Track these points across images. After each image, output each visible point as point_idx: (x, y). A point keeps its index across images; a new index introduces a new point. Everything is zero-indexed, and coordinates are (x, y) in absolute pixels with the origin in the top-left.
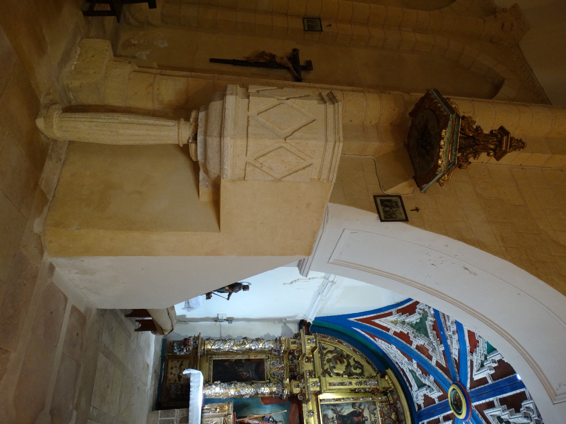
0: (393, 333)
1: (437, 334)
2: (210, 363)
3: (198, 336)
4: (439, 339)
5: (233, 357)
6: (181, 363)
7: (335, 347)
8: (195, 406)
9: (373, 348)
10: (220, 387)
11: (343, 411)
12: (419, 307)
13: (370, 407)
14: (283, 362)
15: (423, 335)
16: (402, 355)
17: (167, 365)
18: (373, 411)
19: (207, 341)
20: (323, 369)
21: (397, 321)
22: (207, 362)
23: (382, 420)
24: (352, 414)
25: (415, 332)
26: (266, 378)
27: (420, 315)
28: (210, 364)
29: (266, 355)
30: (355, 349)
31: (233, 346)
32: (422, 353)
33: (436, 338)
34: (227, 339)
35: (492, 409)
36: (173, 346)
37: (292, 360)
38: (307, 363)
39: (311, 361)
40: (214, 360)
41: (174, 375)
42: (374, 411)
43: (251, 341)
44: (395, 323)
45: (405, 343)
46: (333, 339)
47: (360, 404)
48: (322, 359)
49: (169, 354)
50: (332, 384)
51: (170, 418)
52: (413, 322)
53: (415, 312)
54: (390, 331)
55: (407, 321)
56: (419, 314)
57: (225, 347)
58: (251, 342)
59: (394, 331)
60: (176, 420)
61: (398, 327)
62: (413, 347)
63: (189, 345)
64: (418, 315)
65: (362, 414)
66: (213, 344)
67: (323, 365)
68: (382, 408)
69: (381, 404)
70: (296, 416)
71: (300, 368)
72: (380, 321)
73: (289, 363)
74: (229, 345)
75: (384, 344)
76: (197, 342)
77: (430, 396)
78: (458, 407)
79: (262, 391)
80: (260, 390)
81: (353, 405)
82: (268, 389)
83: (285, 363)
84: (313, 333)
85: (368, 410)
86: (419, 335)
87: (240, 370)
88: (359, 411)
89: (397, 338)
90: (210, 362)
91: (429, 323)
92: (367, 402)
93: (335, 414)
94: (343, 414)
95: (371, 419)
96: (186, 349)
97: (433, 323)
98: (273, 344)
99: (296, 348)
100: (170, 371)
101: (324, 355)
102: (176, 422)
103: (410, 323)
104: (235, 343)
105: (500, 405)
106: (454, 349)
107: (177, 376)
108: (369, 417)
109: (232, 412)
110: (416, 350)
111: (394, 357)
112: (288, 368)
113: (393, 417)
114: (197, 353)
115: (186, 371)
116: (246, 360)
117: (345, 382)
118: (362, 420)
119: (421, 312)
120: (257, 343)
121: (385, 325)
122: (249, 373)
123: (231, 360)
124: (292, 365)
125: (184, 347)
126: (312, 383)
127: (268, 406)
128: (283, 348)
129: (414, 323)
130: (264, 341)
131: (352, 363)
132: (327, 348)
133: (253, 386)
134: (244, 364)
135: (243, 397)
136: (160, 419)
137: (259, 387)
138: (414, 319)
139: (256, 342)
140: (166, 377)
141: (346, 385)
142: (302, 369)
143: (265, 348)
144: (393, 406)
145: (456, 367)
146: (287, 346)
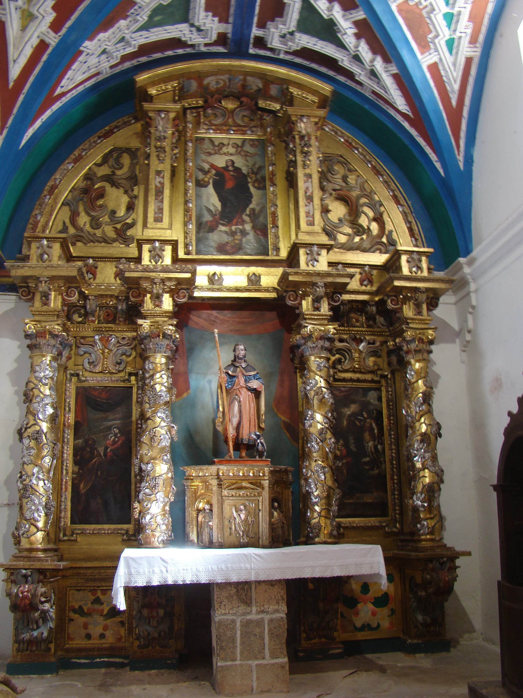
0: (52, 34)
2: (79, 532)
3: (6, 569)
5: (66, 469)
6: (75, 611)
7: (63, 204)
8: (215, 567)
9: (77, 112)
10: (149, 500)
11: (212, 208)
14: (90, 339)
16: (111, 31)
17: (80, 652)
18: (215, 146)
19: (22, 544)
20: (114, 240)
21: (23, 11)
22: (76, 541)
24: (218, 187)
26: (127, 385)
28: (82, 533)
29: (68, 382)
30: (74, 157)
31: (41, 467)
34: (21, 486)
36: (31, 642)
37: (86, 315)
38: (98, 276)
39: (93, 266)
40: (73, 522)
41: (105, 628)
42: (216, 143)
43: (31, 417)
46: (41, 206)
47: (199, 169)
48: (92, 239)
49: (53, 650)
50: (156, 215)
51: (239, 633)
54: (47, 40)
57: (42, 491)
58: (35, 415)
59: (50, 27)
60: (244, 614)
61: (41, 11)
63: (32, 595)
65: (221, 170)
66: (32, 524)
67: (106, 240)
68: (211, 126)
69: (202, 126)
70: (216, 317)
71: (110, 293)
72: (14, 61)
73: (93, 322)
74: (39, 479)
75: (75, 75)
76: (24, 571)
79: (164, 389)
80: (161, 396)
81: (200, 184)
82: (158, 375)
83: (91, 334)
84: (20, 252)
85: (212, 156)
87: (101, 450)
88: (215, 175)
89: (69, 24)
90: (77, 534)
92: (195, 153)
93: (218, 226)
94: (218, 210)
95: (231, 155)
96: (42, 603)
98: (44, 356)
99: (60, 297)
100: (95, 642)
101: (81, 234)
102: (249, 613)
104: (32, 463)
107: (109, 621)
108: (227, 158)
109: (213, 469)
111: (109, 61)
112: (105, 325)
113: (230, 105)
114: (55, 571)
115: (119, 601)
116: (77, 435)
117: (156, 186)
118: (232, 173)
120: (38, 399)
121: (28, 51)
122: (109, 428)
123: (74, 476)
124: (99, 316)
125: (38, 610)
126: (152, 261)
127: (194, 381)
128: (57, 328)
130: (33, 380)
131: (104, 171)
132: (64, 223)
133: (149, 415)
134: (86, 441)
135: (176, 439)
136: (238, 658)
137: (157, 396)
139: (34, 401)
140: (112, 651)
141: (163, 183)
142: (111, 290)
143: (52, 378)
144: (210, 101)
146: (51, 318)
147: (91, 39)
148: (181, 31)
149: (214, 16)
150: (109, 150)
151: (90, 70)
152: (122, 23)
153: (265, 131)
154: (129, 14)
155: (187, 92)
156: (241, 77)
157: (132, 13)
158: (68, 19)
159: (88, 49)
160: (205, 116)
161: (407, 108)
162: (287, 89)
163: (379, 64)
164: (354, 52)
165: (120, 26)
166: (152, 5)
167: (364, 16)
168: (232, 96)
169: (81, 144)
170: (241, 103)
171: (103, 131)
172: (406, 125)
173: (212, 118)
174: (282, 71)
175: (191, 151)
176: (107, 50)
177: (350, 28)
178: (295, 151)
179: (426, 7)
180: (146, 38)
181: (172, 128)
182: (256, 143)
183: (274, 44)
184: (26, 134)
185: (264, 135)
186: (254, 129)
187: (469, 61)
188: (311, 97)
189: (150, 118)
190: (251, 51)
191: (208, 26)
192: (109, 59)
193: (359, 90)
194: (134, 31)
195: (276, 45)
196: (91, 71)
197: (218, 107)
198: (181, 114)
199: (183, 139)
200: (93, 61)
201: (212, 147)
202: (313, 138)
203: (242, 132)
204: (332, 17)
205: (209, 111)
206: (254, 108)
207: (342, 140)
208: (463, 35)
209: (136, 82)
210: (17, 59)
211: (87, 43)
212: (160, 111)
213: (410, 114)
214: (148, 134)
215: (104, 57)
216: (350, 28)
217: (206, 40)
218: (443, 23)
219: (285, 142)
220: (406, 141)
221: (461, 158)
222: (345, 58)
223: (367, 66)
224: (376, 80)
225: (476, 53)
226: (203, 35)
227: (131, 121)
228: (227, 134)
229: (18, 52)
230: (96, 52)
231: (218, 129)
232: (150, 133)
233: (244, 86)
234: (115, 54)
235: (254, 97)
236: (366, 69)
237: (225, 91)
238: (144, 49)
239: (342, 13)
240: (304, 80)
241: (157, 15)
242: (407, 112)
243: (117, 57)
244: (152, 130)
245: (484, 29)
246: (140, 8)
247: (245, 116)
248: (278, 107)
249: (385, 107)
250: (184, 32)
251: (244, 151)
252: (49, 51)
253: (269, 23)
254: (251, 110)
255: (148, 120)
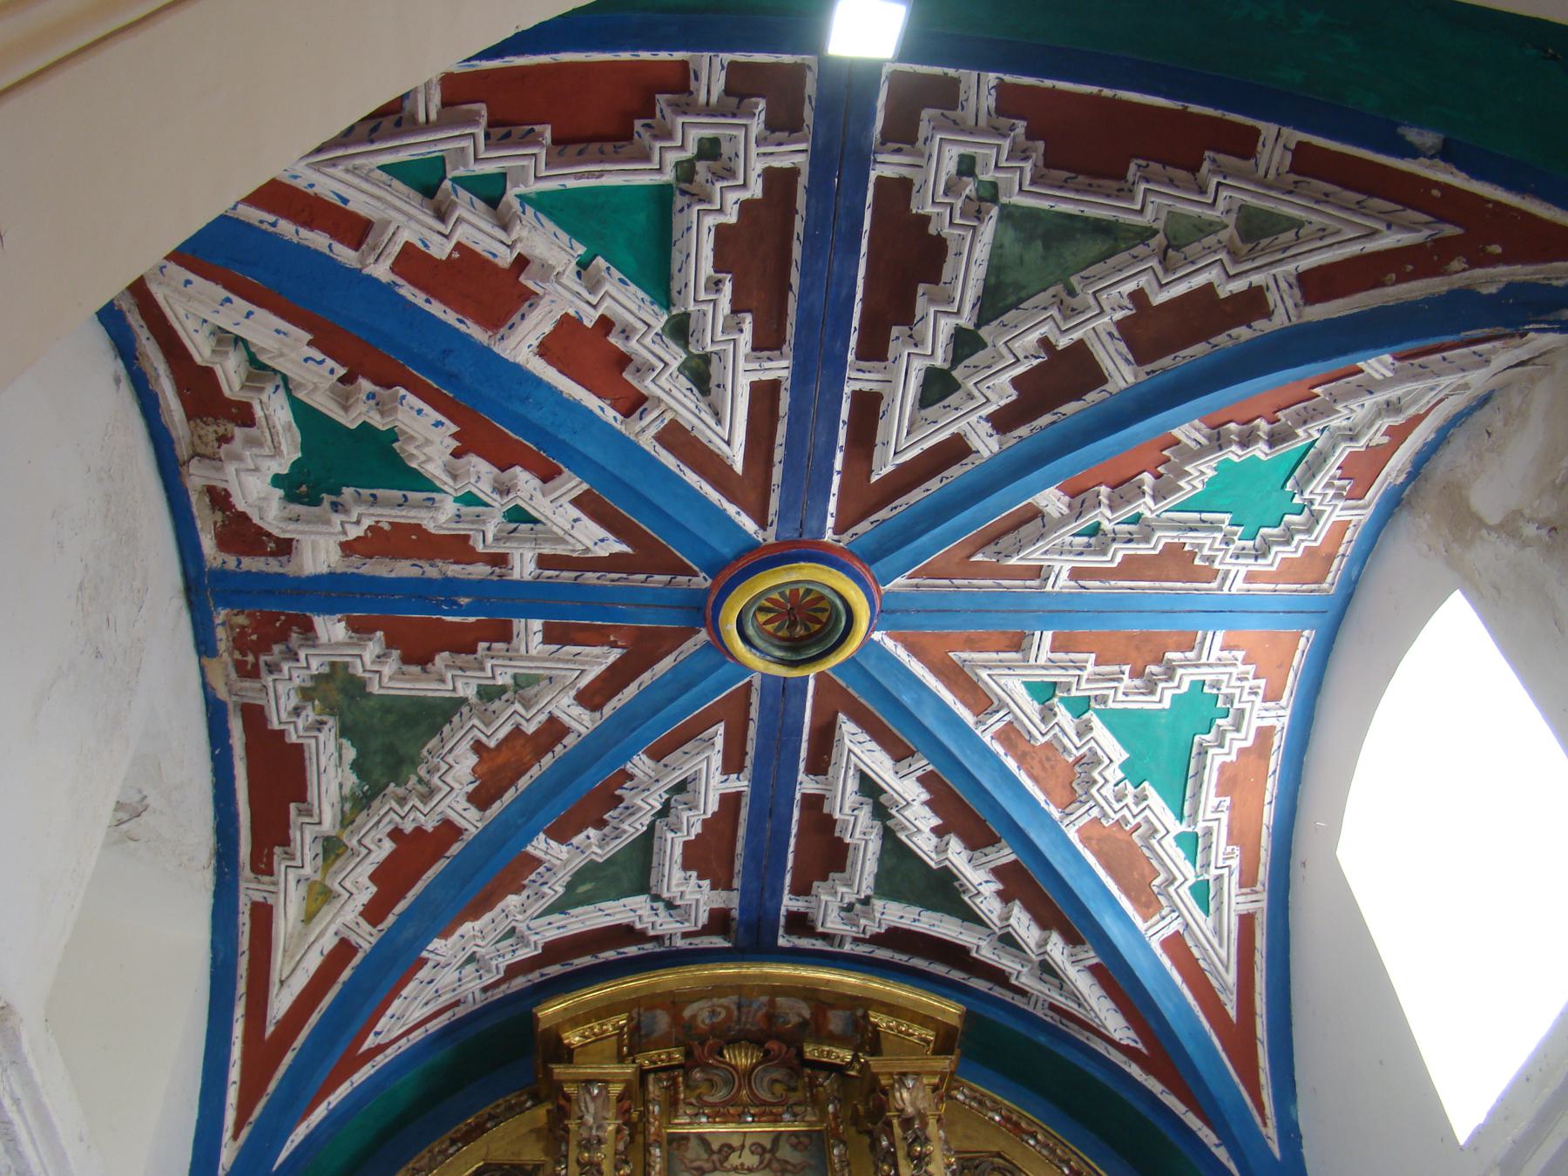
1: (456, 650)
4: (482, 645)
12: (284, 716)
13: (696, 1164)
15: (429, 746)
16: (487, 917)
18: (712, 1152)
23: (753, 1116)
25: (401, 791)
27: (326, 728)
32: (513, 781)
33: (471, 657)
35: (881, 423)
42: (715, 1147)
44: (320, 896)
45: (441, 865)
52: (347, 791)
53: (299, 748)
54: (354, 939)
55: (329, 822)
56: (319, 730)
59: (362, 914)
62: (471, 821)
64: (322, 737)
72: (282, 982)
77: (709, 816)
78: (810, 636)
86: (422, 771)
89: (401, 907)
91: (387, 670)
97: (396, 653)
103: (342, 811)
105: (883, 364)
106: (573, 527)
110: (488, 812)
111: (480, 977)
113: (742, 1059)
119: (310, 714)
121: (313, 962)
129: (352, 779)
138: (332, 770)
144: (697, 1051)
145: (643, 577)
147: (446, 935)
148: (633, 911)
149: (700, 877)
150: (474, 1169)
151: (439, 996)
152: (512, 900)
153: (824, 1112)
154: (526, 882)
155: (647, 1035)
156: (764, 999)
157: (534, 881)
158: (402, 896)
159: (437, 954)
160: (687, 1086)
161: (1132, 1034)
162: (866, 1016)
163: (1057, 949)
164: (1000, 929)
165: (508, 906)
166: (574, 864)
167: (1013, 857)
168: (746, 1039)
169: (411, 1158)
170: (767, 1053)
171: (462, 1127)
172: (1135, 1070)
173: (703, 1089)
174: (850, 980)
175: (658, 1167)
176: (478, 956)
177: (987, 882)
178: (894, 1155)
179: (1138, 826)
180: (559, 928)
181: (616, 1119)
182: (803, 1139)
183: (829, 925)
184: (291, 1138)
185: (821, 1121)
186: (798, 1109)
187: (1246, 921)
188: (918, 1031)
189: (567, 1098)
190: (782, 942)
191: (690, 898)
192: (481, 972)
193: (1022, 1006)
194: (535, 915)
195: (832, 926)
196: (441, 999)
197: (718, 1064)
198: (636, 1085)
199: (640, 1138)
200: (448, 977)
201: (705, 1156)
202: (932, 1122)
203: (772, 1118)
204: (947, 863)
205: (698, 1075)
206: (796, 1062)
207: (997, 1118)
208: (1225, 871)
209: (538, 1019)
210: (287, 978)
211: (436, 944)
212: (589, 1082)
213: (1140, 1046)
214: (562, 1132)
215: (470, 968)
216: (987, 882)
217: (687, 924)
218: (1178, 854)
219: (870, 1133)
220: (1142, 1107)
221: (1271, 1132)
222: (982, 943)
223: (1033, 956)
224: (1057, 982)
225: (1258, 903)
226: (679, 916)
227: (526, 1102)
228: (740, 1123)
229: (293, 964)
230: (454, 961)
231: (719, 1114)
232: (566, 1130)
233: (771, 1017)
234: (494, 963)
235: (794, 1039)
236: (1030, 961)
237: (729, 1029)
238: (555, 951)
239: (965, 854)
240: (901, 996)
241: (583, 882)
242: (1132, 1044)
243: (497, 968)
244: (572, 1125)
245: (1265, 856)
246: (549, 870)
247: (775, 1081)
248: (848, 1056)
249: (1082, 1036)
250: (639, 913)
251: (778, 1160)
252: (356, 961)
253: (816, 884)
254: (791, 1068)
255: (562, 1102)
